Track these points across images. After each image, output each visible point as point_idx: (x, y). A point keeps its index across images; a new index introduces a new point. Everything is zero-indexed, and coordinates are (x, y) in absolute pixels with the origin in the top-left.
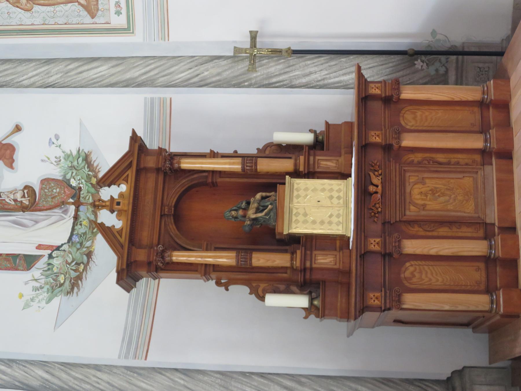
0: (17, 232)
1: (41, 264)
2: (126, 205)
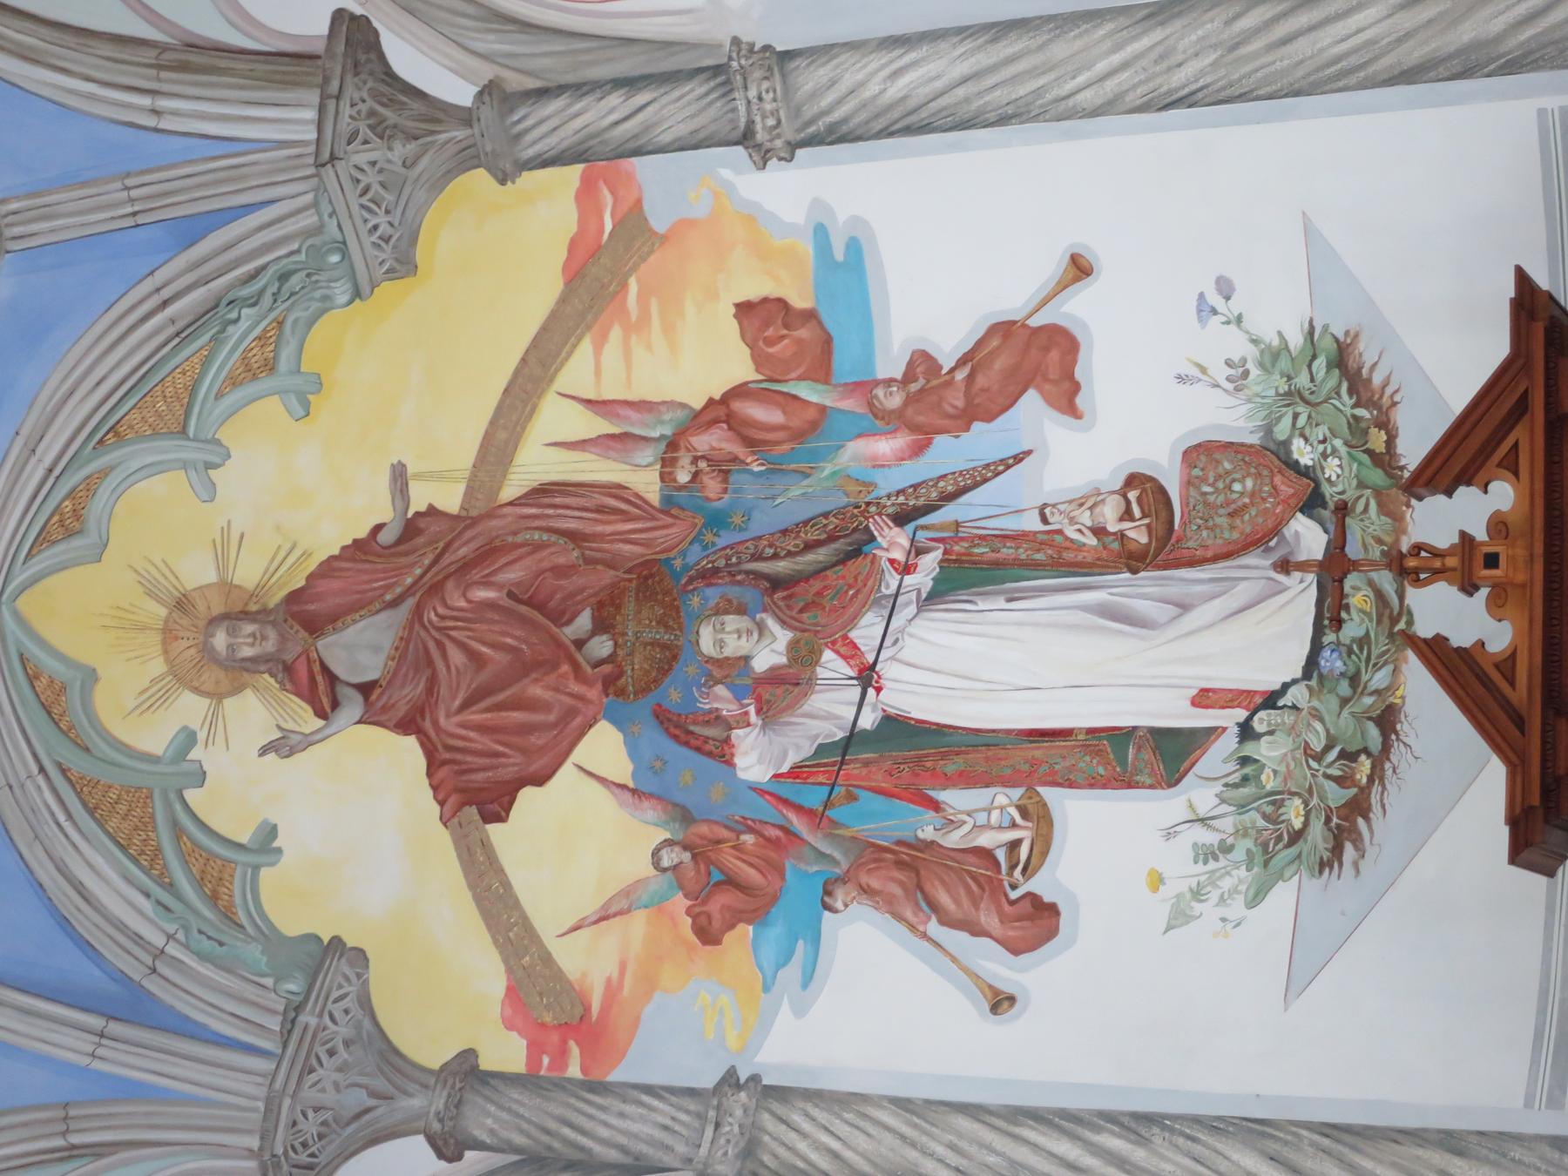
0: (1115, 650)
1: (1217, 759)
2: (1522, 564)
